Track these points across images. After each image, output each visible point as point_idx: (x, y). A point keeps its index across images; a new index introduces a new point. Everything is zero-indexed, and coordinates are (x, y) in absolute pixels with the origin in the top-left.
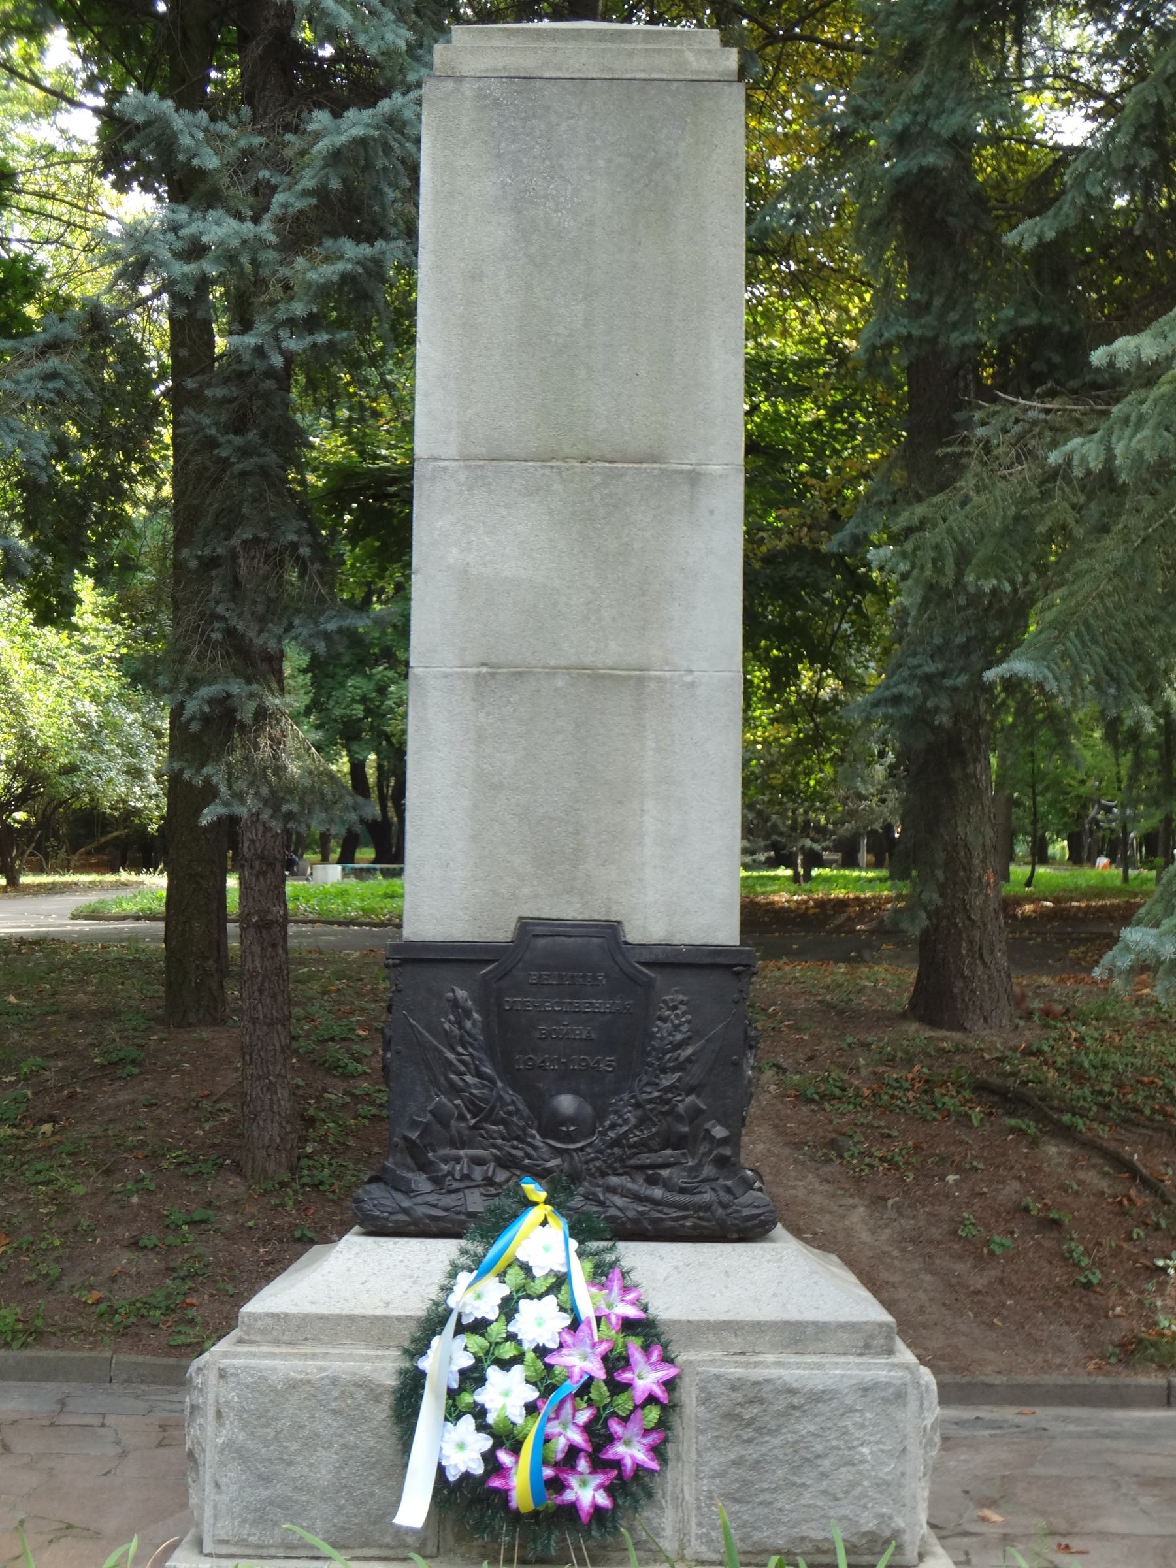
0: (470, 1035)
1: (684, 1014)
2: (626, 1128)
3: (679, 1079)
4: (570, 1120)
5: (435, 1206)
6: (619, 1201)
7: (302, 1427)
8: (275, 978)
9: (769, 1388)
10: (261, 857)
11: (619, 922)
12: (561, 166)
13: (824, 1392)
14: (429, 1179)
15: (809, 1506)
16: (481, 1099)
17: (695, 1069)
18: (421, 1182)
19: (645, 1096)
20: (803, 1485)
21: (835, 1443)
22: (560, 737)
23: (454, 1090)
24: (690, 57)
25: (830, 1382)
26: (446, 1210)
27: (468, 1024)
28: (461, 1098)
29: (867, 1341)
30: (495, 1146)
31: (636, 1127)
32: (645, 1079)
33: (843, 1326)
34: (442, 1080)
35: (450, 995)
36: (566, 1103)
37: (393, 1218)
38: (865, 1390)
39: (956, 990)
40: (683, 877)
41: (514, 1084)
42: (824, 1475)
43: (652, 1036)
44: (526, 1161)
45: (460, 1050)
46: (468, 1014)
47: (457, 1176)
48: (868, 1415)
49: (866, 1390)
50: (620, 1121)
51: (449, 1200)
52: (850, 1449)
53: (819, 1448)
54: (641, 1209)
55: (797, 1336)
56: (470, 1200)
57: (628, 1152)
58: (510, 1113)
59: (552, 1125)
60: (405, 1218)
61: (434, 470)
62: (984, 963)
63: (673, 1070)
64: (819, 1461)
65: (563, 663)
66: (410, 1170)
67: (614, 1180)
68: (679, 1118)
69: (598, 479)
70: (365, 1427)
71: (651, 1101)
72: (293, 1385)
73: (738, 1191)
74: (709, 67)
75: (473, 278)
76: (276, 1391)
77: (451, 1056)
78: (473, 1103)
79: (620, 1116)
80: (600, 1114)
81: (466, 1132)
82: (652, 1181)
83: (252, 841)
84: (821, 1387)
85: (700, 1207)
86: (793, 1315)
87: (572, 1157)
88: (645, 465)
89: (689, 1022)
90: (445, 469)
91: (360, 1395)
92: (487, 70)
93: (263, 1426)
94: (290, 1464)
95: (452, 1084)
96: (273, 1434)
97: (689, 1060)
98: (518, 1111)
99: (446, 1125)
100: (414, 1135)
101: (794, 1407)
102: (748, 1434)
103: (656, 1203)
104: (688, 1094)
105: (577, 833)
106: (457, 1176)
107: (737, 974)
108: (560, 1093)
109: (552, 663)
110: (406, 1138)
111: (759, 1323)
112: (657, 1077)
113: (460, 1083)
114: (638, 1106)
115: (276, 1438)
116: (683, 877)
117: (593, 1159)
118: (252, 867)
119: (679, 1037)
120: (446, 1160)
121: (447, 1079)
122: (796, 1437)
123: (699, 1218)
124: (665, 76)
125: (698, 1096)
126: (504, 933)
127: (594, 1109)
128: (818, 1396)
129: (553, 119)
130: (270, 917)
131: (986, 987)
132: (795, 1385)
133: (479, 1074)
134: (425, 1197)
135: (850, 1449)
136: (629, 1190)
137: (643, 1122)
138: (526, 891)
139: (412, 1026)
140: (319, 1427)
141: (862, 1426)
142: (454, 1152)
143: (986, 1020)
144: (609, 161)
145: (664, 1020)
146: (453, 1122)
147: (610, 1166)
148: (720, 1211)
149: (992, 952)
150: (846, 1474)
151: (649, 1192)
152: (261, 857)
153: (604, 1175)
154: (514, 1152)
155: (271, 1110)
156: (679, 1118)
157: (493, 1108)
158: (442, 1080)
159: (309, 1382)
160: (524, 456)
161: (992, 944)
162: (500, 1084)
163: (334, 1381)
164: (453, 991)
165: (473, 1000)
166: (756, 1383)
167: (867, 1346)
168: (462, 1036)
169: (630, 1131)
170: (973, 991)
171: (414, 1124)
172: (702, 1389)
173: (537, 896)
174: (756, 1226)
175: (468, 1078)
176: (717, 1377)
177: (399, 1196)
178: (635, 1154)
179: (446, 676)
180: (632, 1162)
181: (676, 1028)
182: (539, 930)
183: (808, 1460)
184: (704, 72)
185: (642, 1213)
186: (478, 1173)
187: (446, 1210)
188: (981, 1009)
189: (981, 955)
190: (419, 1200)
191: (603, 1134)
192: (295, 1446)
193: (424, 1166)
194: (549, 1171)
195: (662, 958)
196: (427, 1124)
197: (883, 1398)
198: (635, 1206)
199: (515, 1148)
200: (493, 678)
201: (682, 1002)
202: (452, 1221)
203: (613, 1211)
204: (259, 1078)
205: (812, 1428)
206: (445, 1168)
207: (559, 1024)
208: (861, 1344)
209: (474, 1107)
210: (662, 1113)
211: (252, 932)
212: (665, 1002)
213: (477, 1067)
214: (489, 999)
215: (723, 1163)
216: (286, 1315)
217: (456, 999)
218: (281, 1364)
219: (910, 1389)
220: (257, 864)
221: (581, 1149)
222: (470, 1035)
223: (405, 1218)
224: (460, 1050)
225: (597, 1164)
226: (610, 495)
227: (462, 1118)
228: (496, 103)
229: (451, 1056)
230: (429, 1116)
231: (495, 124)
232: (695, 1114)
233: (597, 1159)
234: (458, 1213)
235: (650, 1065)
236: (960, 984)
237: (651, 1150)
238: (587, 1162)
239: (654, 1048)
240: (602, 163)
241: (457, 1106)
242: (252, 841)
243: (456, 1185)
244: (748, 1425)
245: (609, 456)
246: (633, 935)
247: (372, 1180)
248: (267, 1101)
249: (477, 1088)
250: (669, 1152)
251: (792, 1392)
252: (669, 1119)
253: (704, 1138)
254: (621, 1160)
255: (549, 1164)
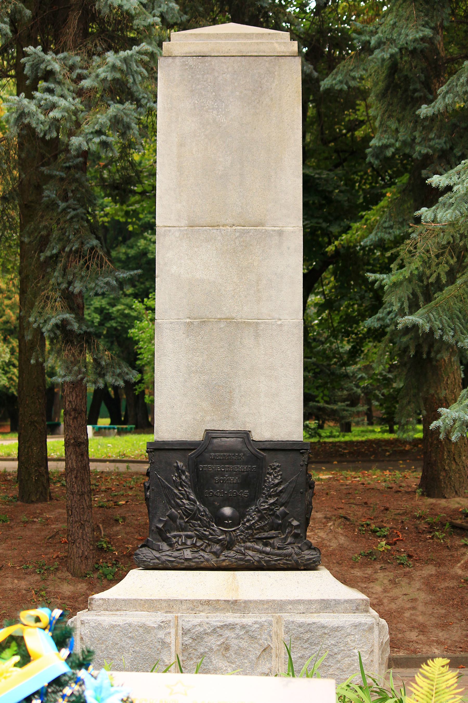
0: (185, 482)
1: (279, 471)
2: (253, 521)
3: (277, 500)
4: (228, 518)
5: (170, 556)
6: (251, 553)
7: (117, 644)
8: (83, 471)
9: (315, 626)
10: (75, 410)
11: (250, 431)
12: (220, 95)
13: (338, 627)
14: (168, 545)
15: (332, 674)
16: (189, 510)
17: (285, 496)
18: (165, 546)
19: (262, 508)
20: (330, 666)
21: (342, 648)
22: (222, 350)
23: (178, 506)
24: (276, 45)
25: (341, 623)
26: (175, 558)
27: (184, 477)
28: (181, 509)
29: (357, 608)
30: (196, 530)
31: (258, 521)
32: (262, 500)
33: (347, 601)
34: (173, 502)
35: (175, 464)
36: (227, 511)
37: (152, 561)
38: (356, 626)
39: (441, 477)
40: (274, 409)
41: (203, 502)
42: (338, 661)
43: (265, 481)
44: (210, 537)
45: (180, 488)
46: (183, 472)
47: (180, 543)
48: (357, 636)
49: (356, 626)
50: (251, 518)
51: (176, 554)
52: (349, 650)
53: (336, 650)
54: (260, 556)
55: (326, 605)
56: (185, 553)
57: (255, 532)
58: (203, 516)
59: (220, 520)
60: (157, 561)
61: (165, 231)
62: (456, 462)
63: (274, 496)
64: (336, 656)
65: (223, 316)
66: (160, 542)
67: (249, 544)
68: (277, 517)
69: (238, 234)
70: (143, 644)
71: (265, 509)
72: (113, 627)
73: (304, 548)
74: (285, 50)
75: (181, 145)
76: (106, 629)
77: (176, 491)
78: (186, 511)
79: (251, 516)
80: (243, 516)
81: (184, 524)
82: (266, 545)
83: (70, 402)
84: (337, 625)
85: (286, 555)
86: (325, 597)
87: (230, 535)
88: (258, 228)
89: (281, 475)
90: (170, 231)
91: (141, 630)
92: (186, 53)
93: (100, 644)
94: (112, 659)
95: (177, 504)
96: (105, 647)
97: (281, 491)
98: (206, 515)
99: (175, 521)
100: (160, 526)
101: (325, 634)
102: (306, 645)
103: (267, 554)
104: (281, 507)
105: (231, 392)
106: (180, 543)
107: (302, 453)
108: (224, 506)
109: (219, 316)
110: (157, 528)
111: (311, 600)
112: (267, 499)
113: (181, 503)
114: (259, 511)
115: (106, 649)
116: (274, 409)
117: (240, 535)
118: (70, 415)
119: (277, 481)
120: (175, 537)
121: (175, 501)
122: (326, 646)
123: (287, 560)
124: (265, 54)
125: (286, 507)
126: (199, 437)
127: (239, 513)
128: (337, 629)
129: (216, 74)
130: (80, 440)
131: (457, 475)
132: (326, 625)
133: (189, 499)
134: (167, 553)
135: (349, 650)
136: (256, 549)
137: (261, 518)
138: (208, 418)
139: (159, 478)
140: (124, 644)
141: (354, 641)
142: (179, 533)
143: (456, 492)
144: (241, 92)
145: (270, 474)
146: (178, 521)
147: (247, 538)
148: (295, 557)
149: (460, 457)
150: (347, 661)
151: (264, 549)
152: (75, 410)
153: (244, 542)
154: (205, 532)
155: (83, 538)
156: (277, 517)
157: (195, 514)
158: (173, 502)
159: (119, 625)
160: (205, 225)
161: (460, 452)
162: (198, 503)
163: (130, 625)
164: (177, 463)
165: (186, 466)
166: (309, 624)
167: (357, 609)
168: (181, 482)
169: (255, 522)
170: (450, 478)
171: (160, 521)
172: (286, 627)
173: (213, 420)
174: (311, 563)
175: (184, 501)
176: (293, 622)
177: (154, 552)
178: (258, 533)
179: (171, 323)
180: (256, 536)
181: (275, 477)
182: (214, 435)
183: (332, 655)
184: (283, 52)
185: (262, 558)
186: (189, 542)
187: (175, 558)
188: (454, 487)
189: (454, 458)
190: (164, 554)
191: (244, 524)
192: (114, 652)
193: (166, 540)
194: (220, 540)
195: (268, 447)
196: (166, 521)
197: (363, 630)
198: (258, 555)
199: (205, 531)
200: (197, 325)
201: (278, 466)
202: (178, 563)
203: (248, 558)
204: (76, 522)
205: (333, 642)
206: (174, 540)
207: (223, 476)
208: (355, 608)
209: (187, 513)
210: (270, 515)
211: (71, 448)
212: (271, 466)
213: (188, 496)
214: (194, 466)
215: (296, 536)
216: (109, 599)
217: (178, 466)
218: (107, 619)
219: (375, 626)
220: (73, 413)
221: (234, 531)
222: (185, 482)
223: (157, 561)
224: (180, 488)
225: (241, 537)
226: (243, 241)
227: (181, 518)
228: (191, 68)
229: (176, 491)
230: (167, 518)
231: (190, 77)
232: (285, 515)
233: (242, 535)
234: (181, 559)
235: (264, 494)
236: (443, 474)
237: (265, 531)
238: (237, 536)
239: (266, 486)
240: (238, 93)
241: (179, 513)
242: (70, 402)
243: (180, 547)
244: (306, 642)
245: (243, 224)
246: (256, 436)
247: (142, 546)
248: (80, 534)
249: (188, 505)
250: (273, 532)
251: (324, 627)
252: (273, 517)
253: (288, 526)
254: (252, 535)
255: (221, 537)
